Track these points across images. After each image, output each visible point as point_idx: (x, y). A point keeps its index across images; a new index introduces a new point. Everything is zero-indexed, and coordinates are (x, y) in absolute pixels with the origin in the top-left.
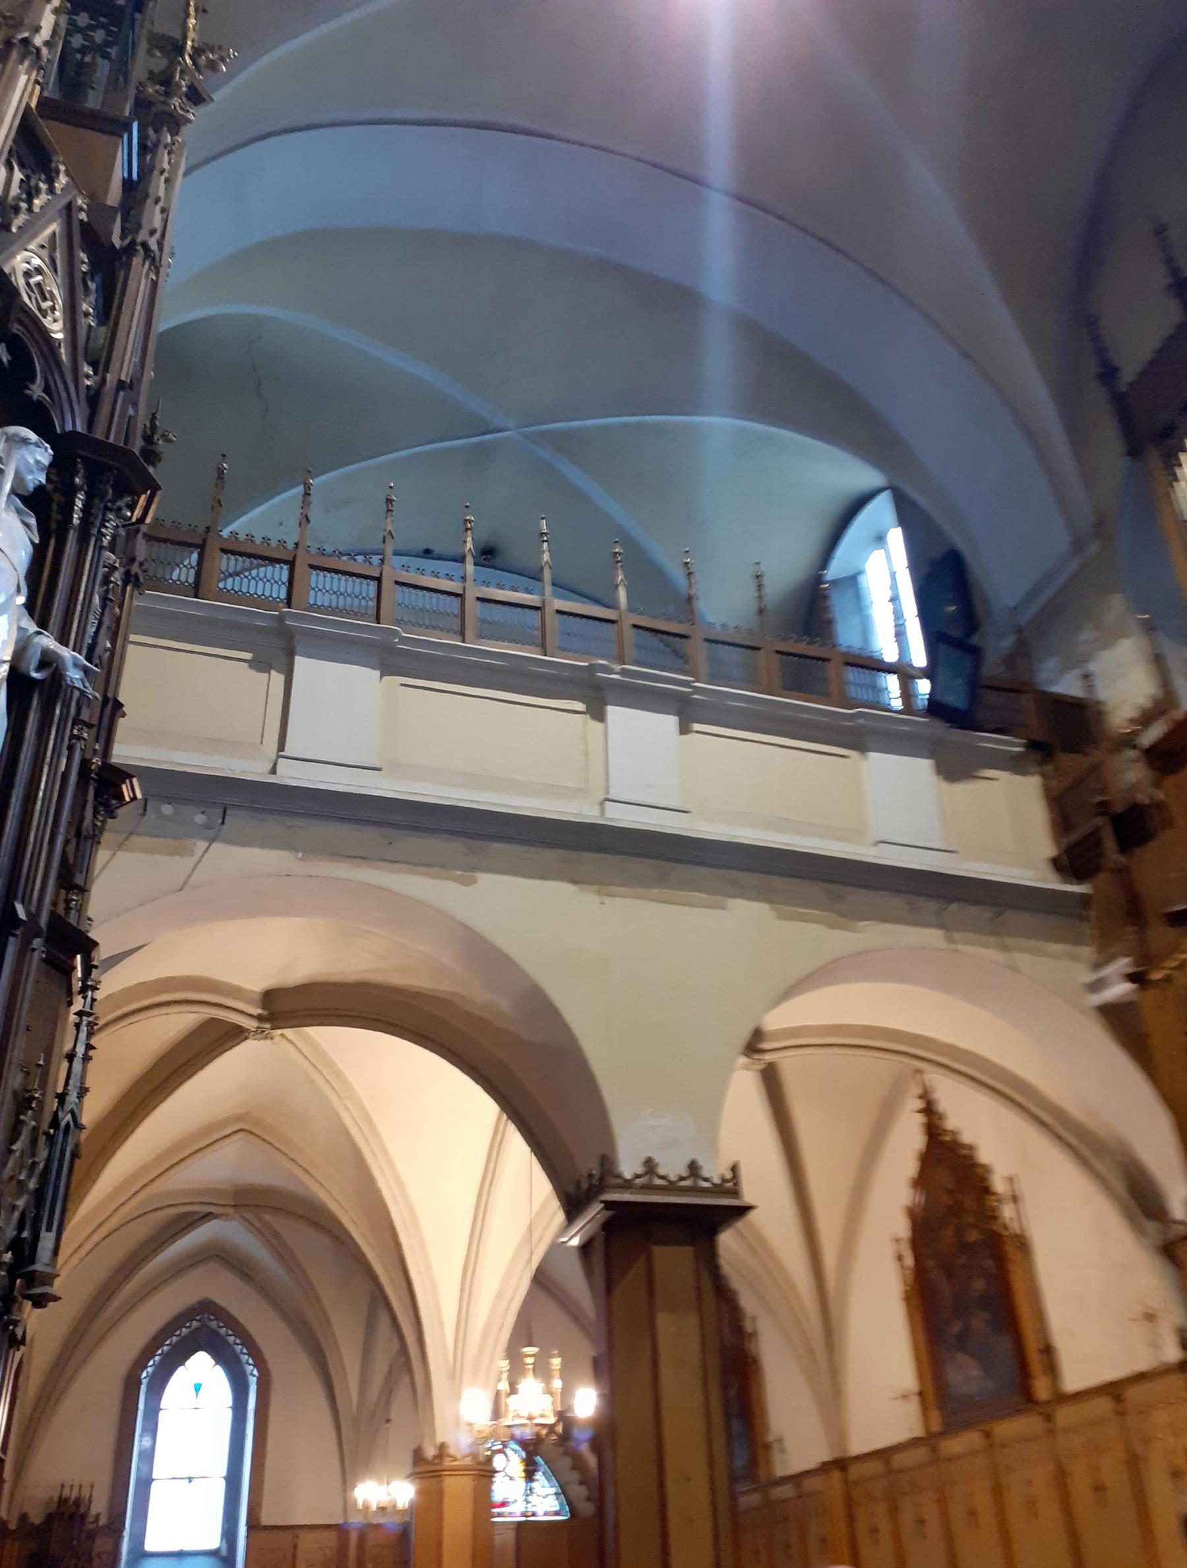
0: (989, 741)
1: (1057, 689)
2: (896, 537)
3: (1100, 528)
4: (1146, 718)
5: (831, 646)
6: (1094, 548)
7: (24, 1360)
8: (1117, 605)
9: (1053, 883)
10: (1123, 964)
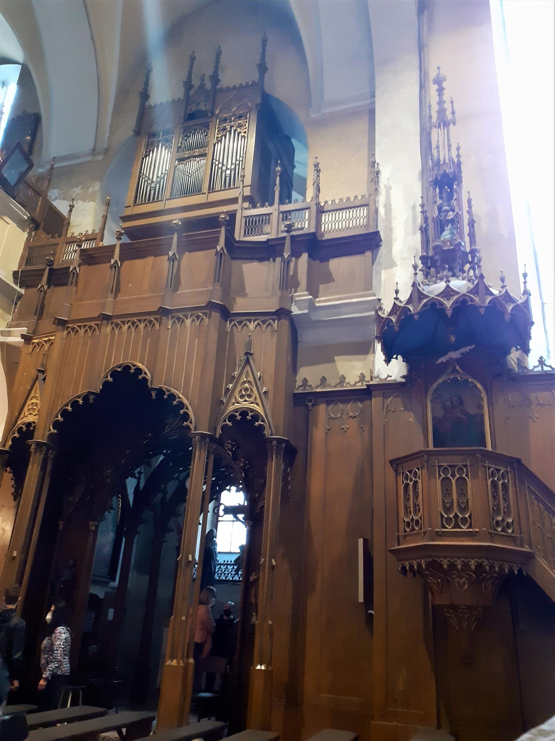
1: (55, 203)
3: (107, 151)
4: (89, 238)
6: (100, 158)
7: (537, 251)
8: (97, 186)
9: (10, 281)
10: (24, 330)
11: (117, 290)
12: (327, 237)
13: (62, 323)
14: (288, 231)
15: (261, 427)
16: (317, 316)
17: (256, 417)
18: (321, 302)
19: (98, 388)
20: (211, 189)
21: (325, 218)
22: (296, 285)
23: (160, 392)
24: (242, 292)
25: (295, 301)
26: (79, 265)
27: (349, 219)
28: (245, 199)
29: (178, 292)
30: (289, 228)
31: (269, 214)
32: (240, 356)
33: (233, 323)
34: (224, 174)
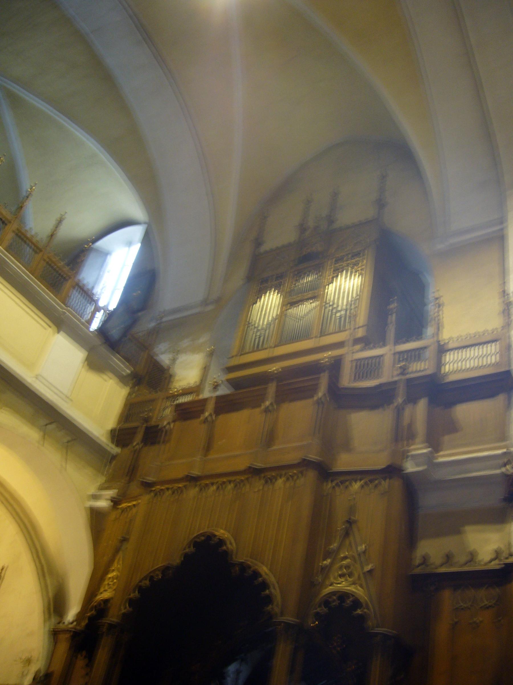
0: (116, 361)
2: (137, 247)
3: (218, 300)
4: (186, 392)
5: (125, 509)
6: (210, 307)
10: (111, 493)
11: (208, 448)
12: (452, 378)
13: (147, 486)
14: (402, 374)
15: (362, 618)
16: (440, 475)
17: (357, 603)
18: (443, 457)
19: (177, 560)
20: (323, 333)
21: (449, 357)
22: (411, 436)
23: (244, 567)
24: (347, 447)
25: (413, 456)
26: (174, 421)
27: (478, 357)
28: (356, 341)
29: (275, 448)
30: (404, 371)
31: (382, 356)
32: (340, 526)
33: (335, 482)
34: (334, 316)
